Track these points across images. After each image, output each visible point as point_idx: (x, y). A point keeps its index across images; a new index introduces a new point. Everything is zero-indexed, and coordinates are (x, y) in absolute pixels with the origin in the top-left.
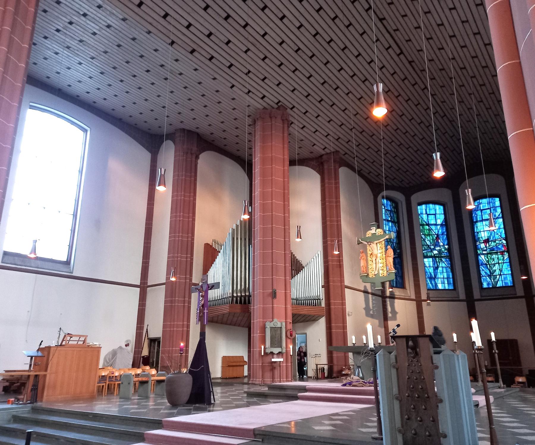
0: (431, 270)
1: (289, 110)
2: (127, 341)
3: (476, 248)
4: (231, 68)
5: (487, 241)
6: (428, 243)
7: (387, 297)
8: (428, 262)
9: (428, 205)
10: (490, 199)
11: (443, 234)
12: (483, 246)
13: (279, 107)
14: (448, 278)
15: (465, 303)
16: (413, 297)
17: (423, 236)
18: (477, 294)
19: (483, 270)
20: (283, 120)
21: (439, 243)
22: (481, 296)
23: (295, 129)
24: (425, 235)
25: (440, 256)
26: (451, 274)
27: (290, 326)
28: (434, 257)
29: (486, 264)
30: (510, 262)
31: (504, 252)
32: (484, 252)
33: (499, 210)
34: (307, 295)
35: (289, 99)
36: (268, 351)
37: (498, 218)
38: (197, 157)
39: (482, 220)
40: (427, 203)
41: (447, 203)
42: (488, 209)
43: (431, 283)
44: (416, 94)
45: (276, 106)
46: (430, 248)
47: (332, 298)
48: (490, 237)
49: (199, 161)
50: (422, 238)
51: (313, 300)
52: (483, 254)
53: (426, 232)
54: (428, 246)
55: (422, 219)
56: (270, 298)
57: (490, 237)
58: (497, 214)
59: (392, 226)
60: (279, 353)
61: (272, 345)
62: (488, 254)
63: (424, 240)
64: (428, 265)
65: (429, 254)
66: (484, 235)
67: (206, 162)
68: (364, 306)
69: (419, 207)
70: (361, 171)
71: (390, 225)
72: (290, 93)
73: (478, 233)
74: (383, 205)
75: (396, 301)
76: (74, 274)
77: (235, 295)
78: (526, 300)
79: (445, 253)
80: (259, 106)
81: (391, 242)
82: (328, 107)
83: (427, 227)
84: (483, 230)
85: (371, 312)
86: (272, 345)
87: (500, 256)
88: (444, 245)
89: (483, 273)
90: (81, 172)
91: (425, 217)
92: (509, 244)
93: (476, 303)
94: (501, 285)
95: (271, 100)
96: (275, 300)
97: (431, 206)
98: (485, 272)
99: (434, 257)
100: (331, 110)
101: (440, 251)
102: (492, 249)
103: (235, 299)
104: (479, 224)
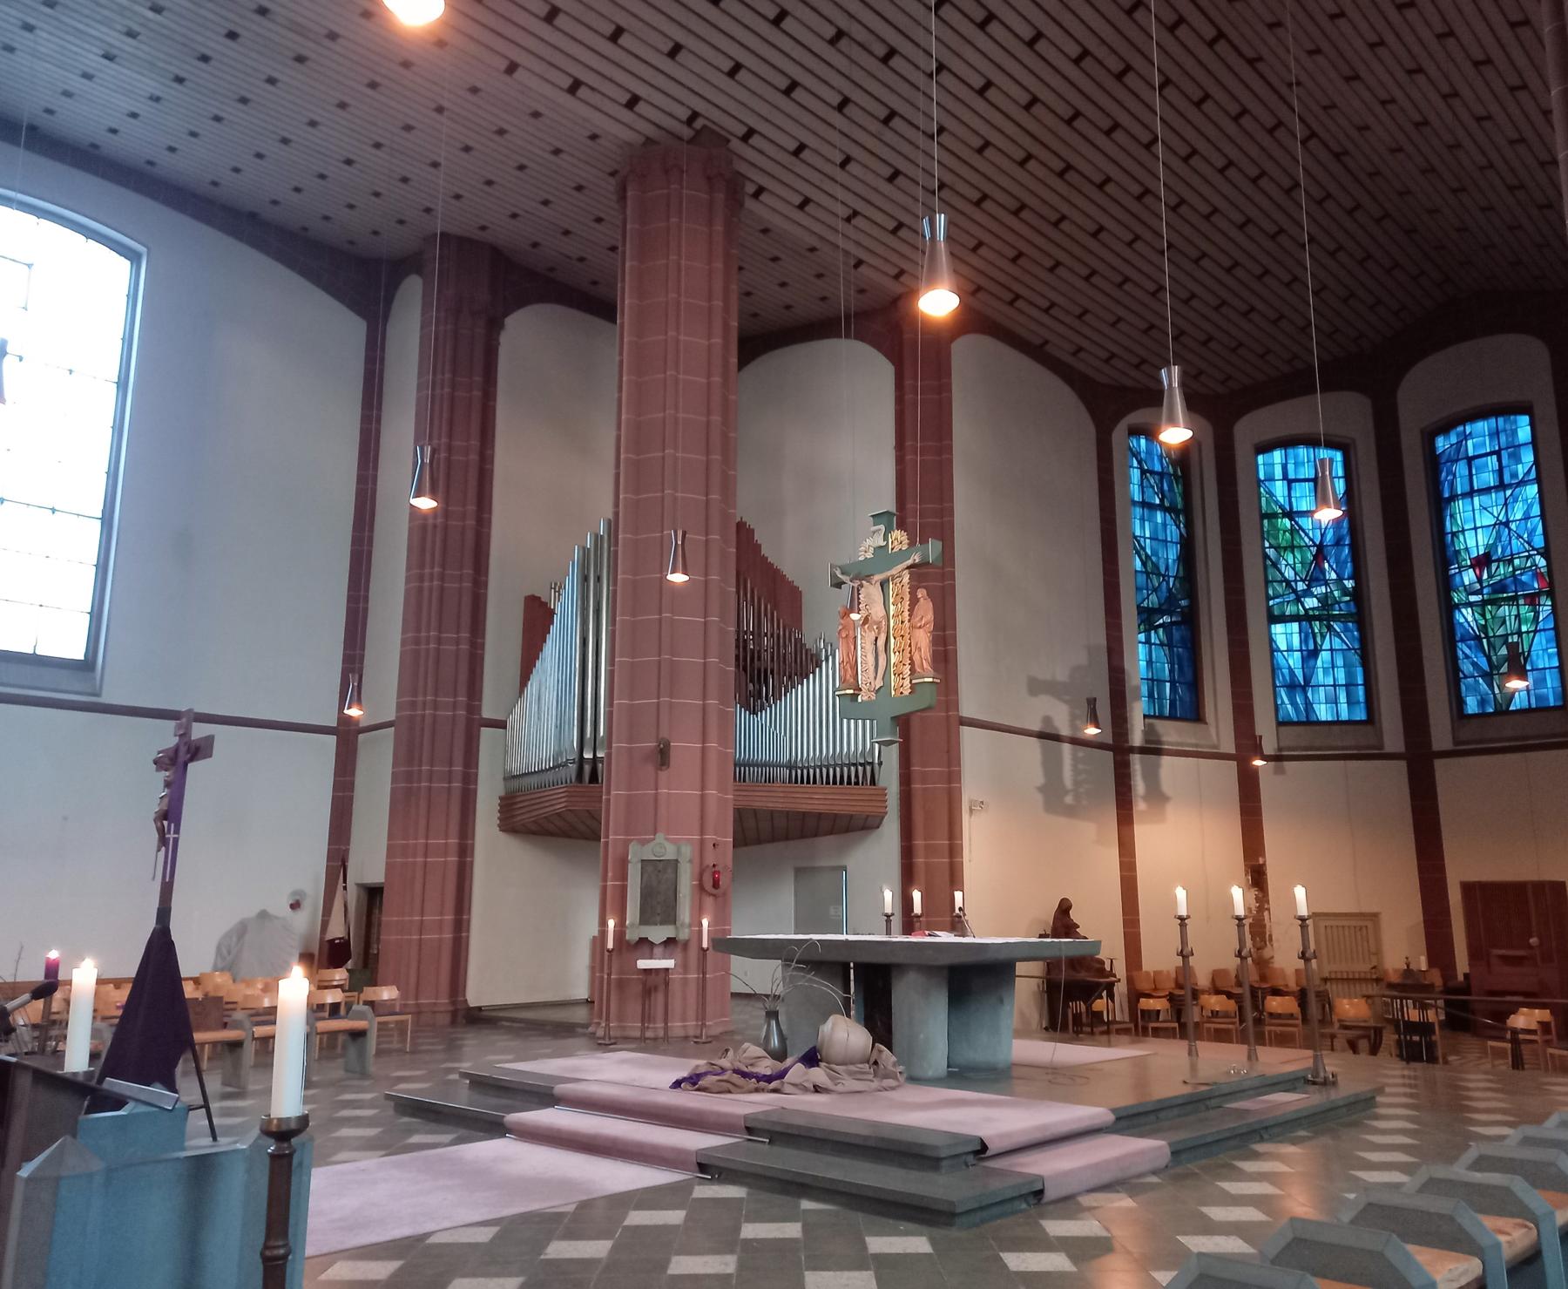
0: (1295, 660)
1: (736, 144)
2: (295, 893)
3: (1446, 585)
4: (613, 27)
5: (1482, 562)
6: (1289, 574)
7: (1132, 750)
8: (1285, 635)
9: (1290, 451)
10: (1501, 420)
11: (1338, 542)
12: (1469, 577)
13: (698, 132)
14: (1349, 686)
15: (1403, 764)
16: (1229, 746)
17: (1271, 552)
18: (1441, 735)
19: (1467, 657)
20: (709, 178)
21: (1323, 571)
22: (1456, 743)
23: (772, 211)
24: (1277, 548)
25: (1325, 614)
26: (1359, 672)
27: (725, 855)
28: (1305, 618)
29: (1478, 639)
30: (1556, 628)
31: (1538, 594)
32: (1473, 598)
33: (1528, 457)
34: (827, 750)
35: (730, 107)
36: (632, 936)
37: (1522, 483)
38: (494, 326)
39: (1471, 493)
40: (1287, 443)
41: (1354, 440)
42: (1491, 454)
43: (1294, 703)
44: (1189, 64)
45: (687, 132)
46: (1295, 591)
47: (915, 758)
48: (1494, 545)
49: (505, 339)
50: (1266, 556)
51: (849, 766)
52: (1471, 605)
53: (1284, 539)
54: (1288, 582)
55: (1271, 494)
56: (650, 768)
57: (1494, 545)
58: (1521, 470)
59: (1164, 525)
60: (670, 942)
61: (646, 919)
62: (1484, 603)
63: (1275, 565)
64: (1283, 647)
65: (1290, 610)
66: (1474, 543)
67: (527, 336)
68: (1039, 778)
69: (1260, 458)
70: (1048, 348)
71: (1159, 520)
72: (724, 82)
73: (1454, 534)
74: (1136, 455)
75: (1166, 761)
76: (107, 698)
77: (588, 755)
78: (1409, 767)
79: (1344, 604)
80: (627, 135)
81: (1159, 574)
82: (875, 127)
83: (1287, 522)
84: (1472, 527)
85: (1069, 799)
86: (646, 919)
87: (1524, 610)
88: (1340, 579)
89: (1466, 667)
90: (122, 384)
91: (1279, 489)
92: (1555, 567)
93: (1439, 764)
94: (1525, 705)
95: (664, 109)
96: (663, 775)
97: (1302, 452)
98: (1474, 664)
99: (1305, 618)
100: (888, 136)
101: (1325, 600)
102: (1500, 587)
103: (587, 768)
104: (1460, 504)
